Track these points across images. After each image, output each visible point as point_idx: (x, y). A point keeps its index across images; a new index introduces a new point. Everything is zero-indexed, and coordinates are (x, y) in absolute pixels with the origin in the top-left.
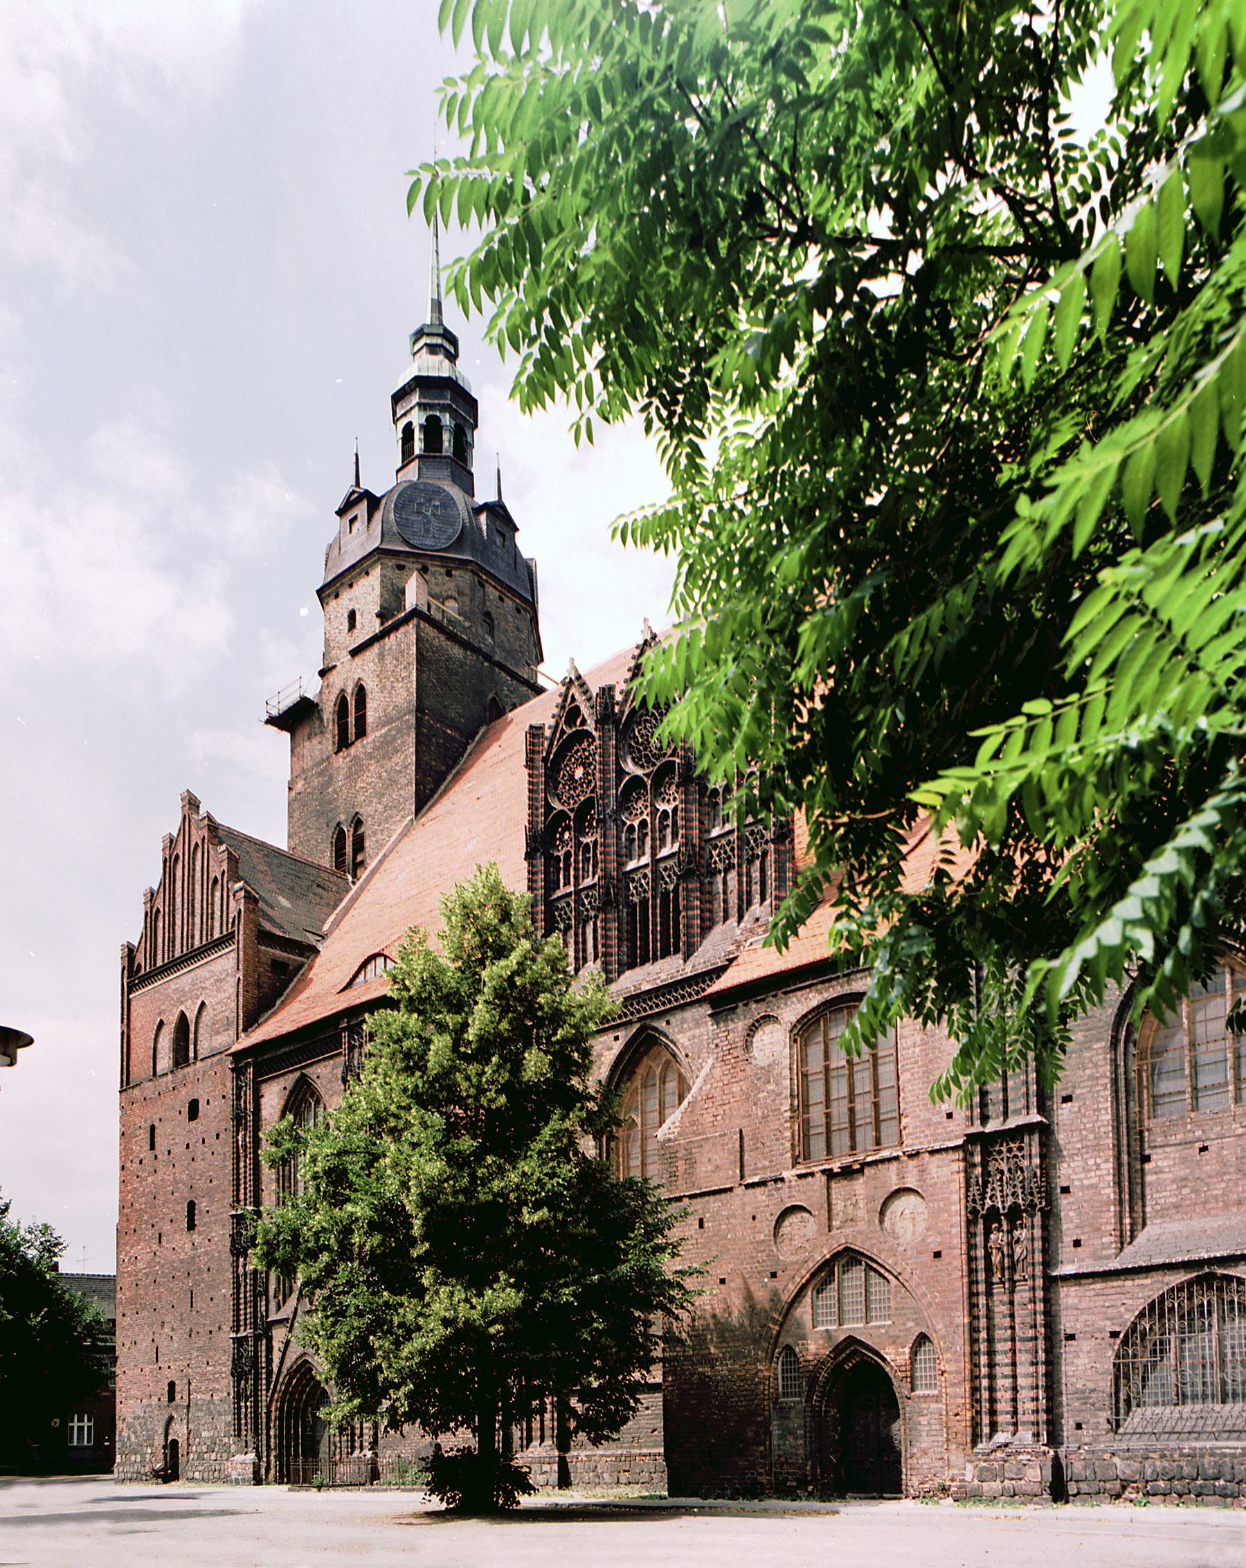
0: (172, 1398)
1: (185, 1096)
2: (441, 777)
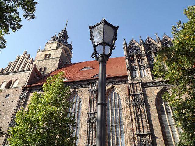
1: (6, 93)
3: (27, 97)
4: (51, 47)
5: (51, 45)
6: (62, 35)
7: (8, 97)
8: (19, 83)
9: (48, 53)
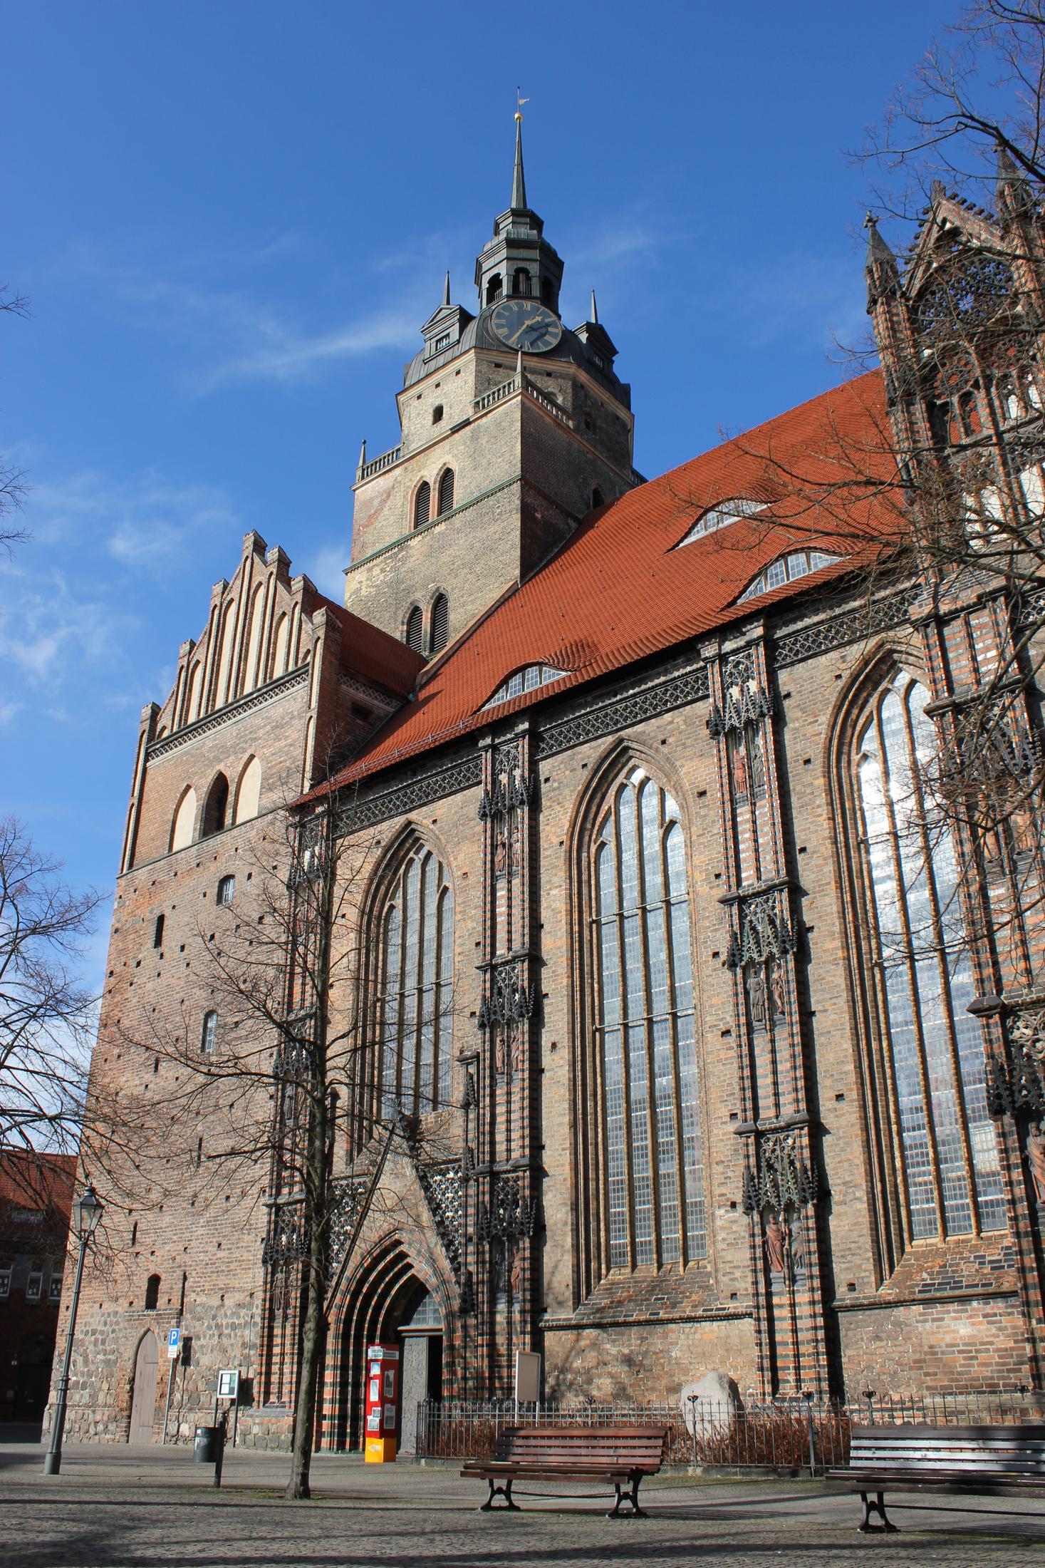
0: (151, 1303)
1: (215, 872)
2: (535, 565)
3: (328, 870)
4: (438, 414)
6: (275, 571)
7: (230, 890)
8: (266, 787)
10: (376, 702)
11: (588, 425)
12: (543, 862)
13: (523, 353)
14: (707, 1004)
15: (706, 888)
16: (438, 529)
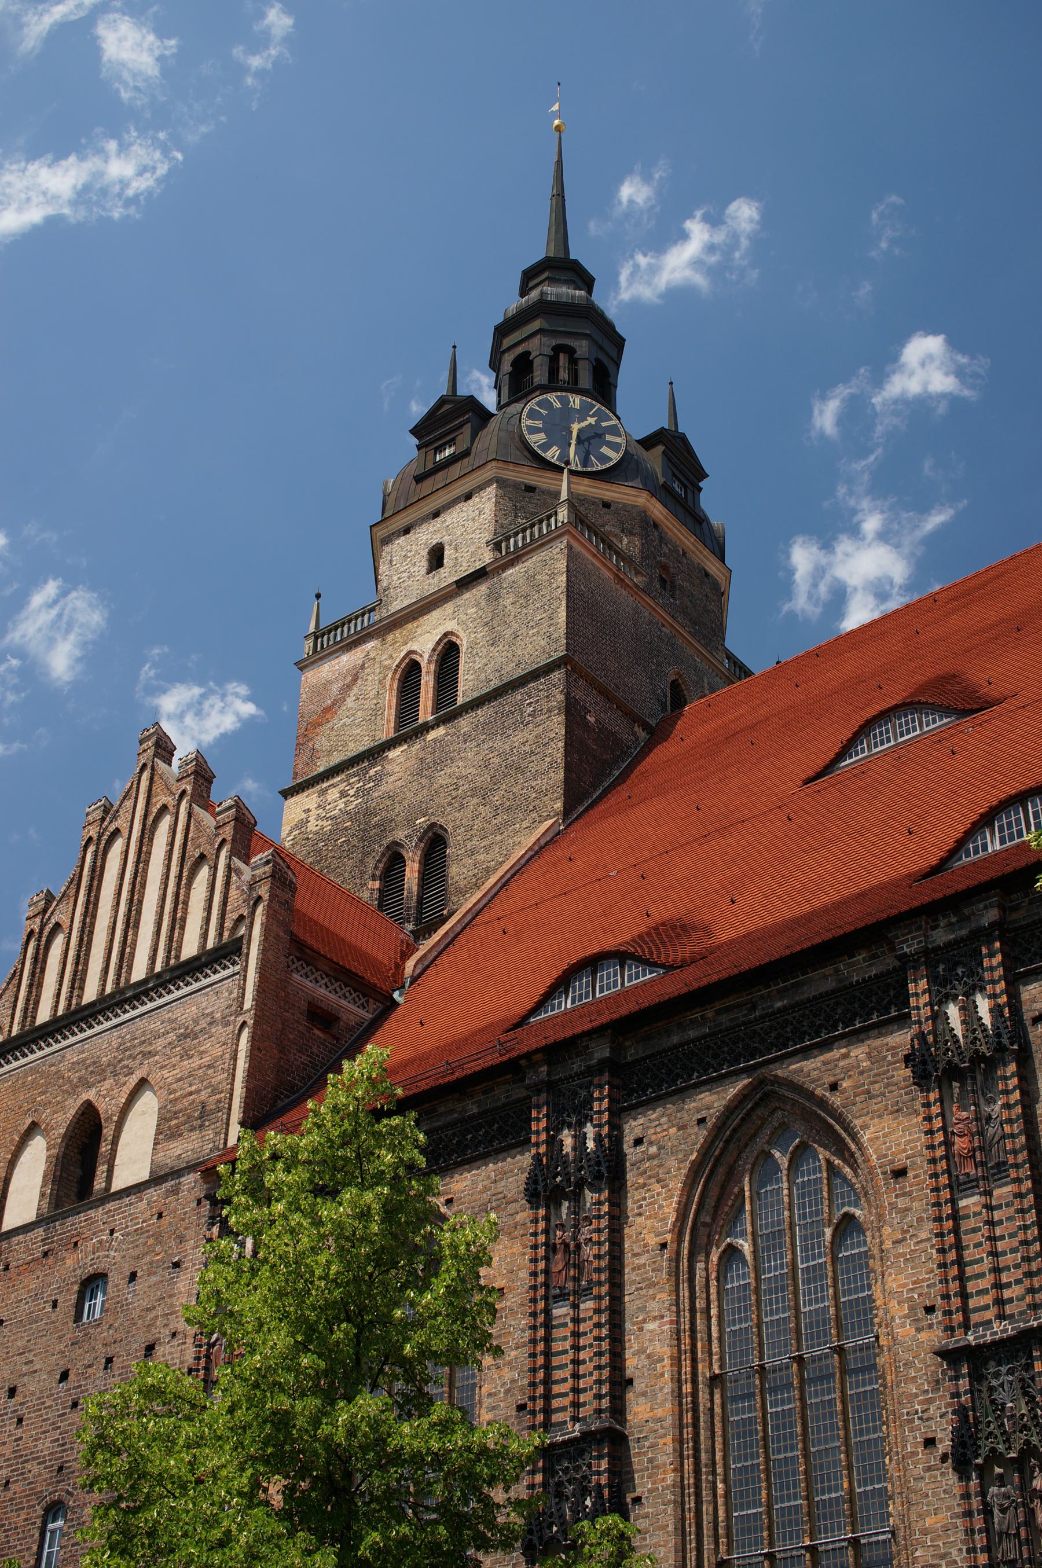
1: (74, 1265)
4: (436, 558)
5: (426, 536)
6: (189, 788)
8: (167, 1130)
9: (423, 640)
10: (344, 1003)
11: (663, 581)
12: (630, 1276)
13: (572, 472)
14: (917, 1527)
15: (909, 1329)
16: (432, 735)
